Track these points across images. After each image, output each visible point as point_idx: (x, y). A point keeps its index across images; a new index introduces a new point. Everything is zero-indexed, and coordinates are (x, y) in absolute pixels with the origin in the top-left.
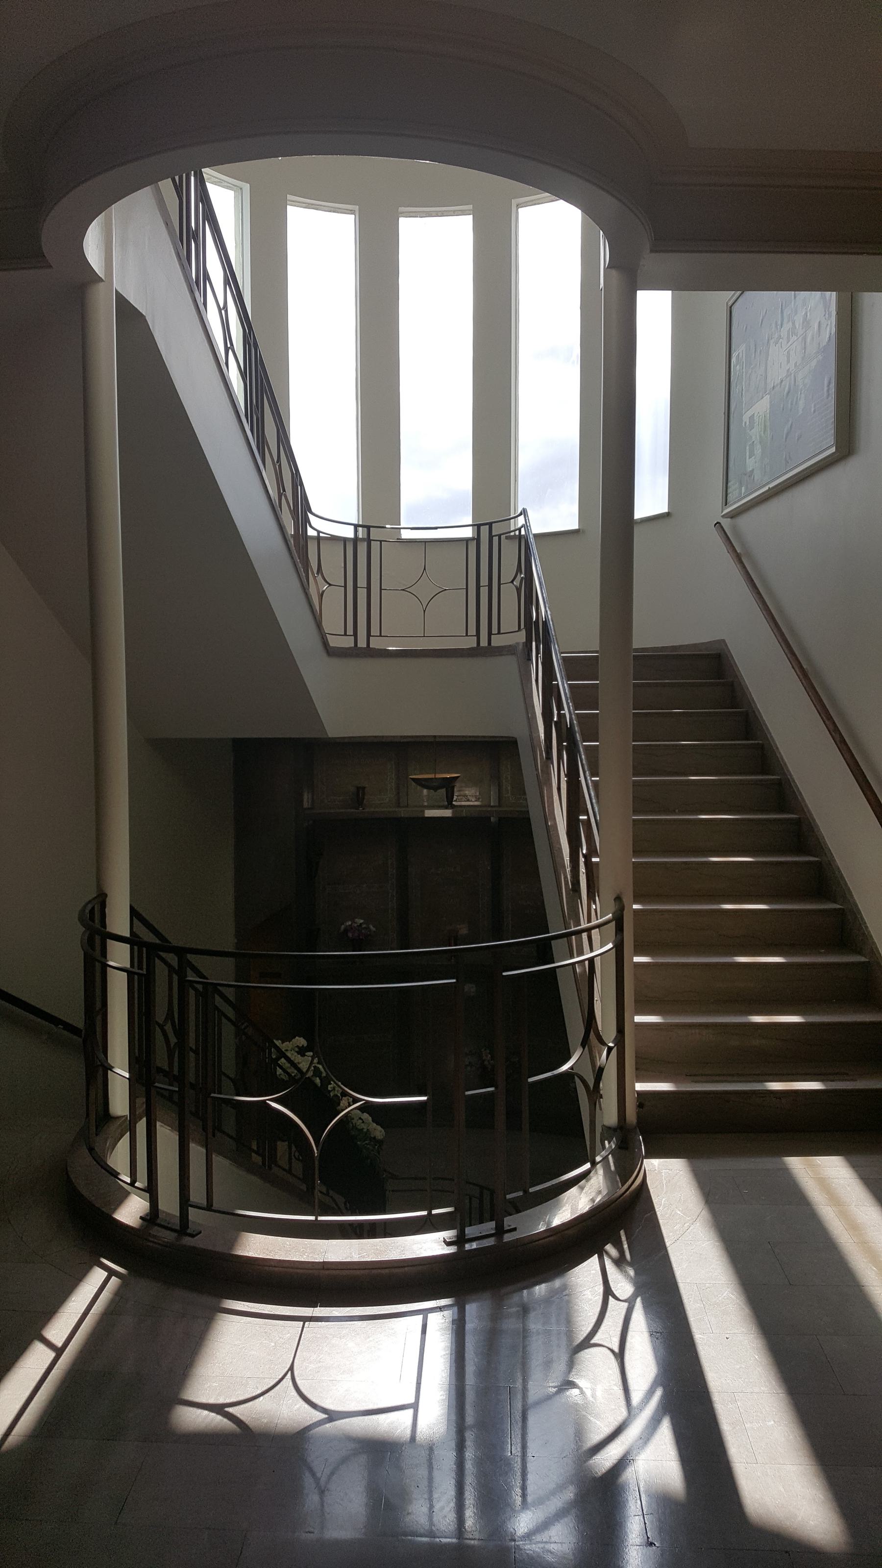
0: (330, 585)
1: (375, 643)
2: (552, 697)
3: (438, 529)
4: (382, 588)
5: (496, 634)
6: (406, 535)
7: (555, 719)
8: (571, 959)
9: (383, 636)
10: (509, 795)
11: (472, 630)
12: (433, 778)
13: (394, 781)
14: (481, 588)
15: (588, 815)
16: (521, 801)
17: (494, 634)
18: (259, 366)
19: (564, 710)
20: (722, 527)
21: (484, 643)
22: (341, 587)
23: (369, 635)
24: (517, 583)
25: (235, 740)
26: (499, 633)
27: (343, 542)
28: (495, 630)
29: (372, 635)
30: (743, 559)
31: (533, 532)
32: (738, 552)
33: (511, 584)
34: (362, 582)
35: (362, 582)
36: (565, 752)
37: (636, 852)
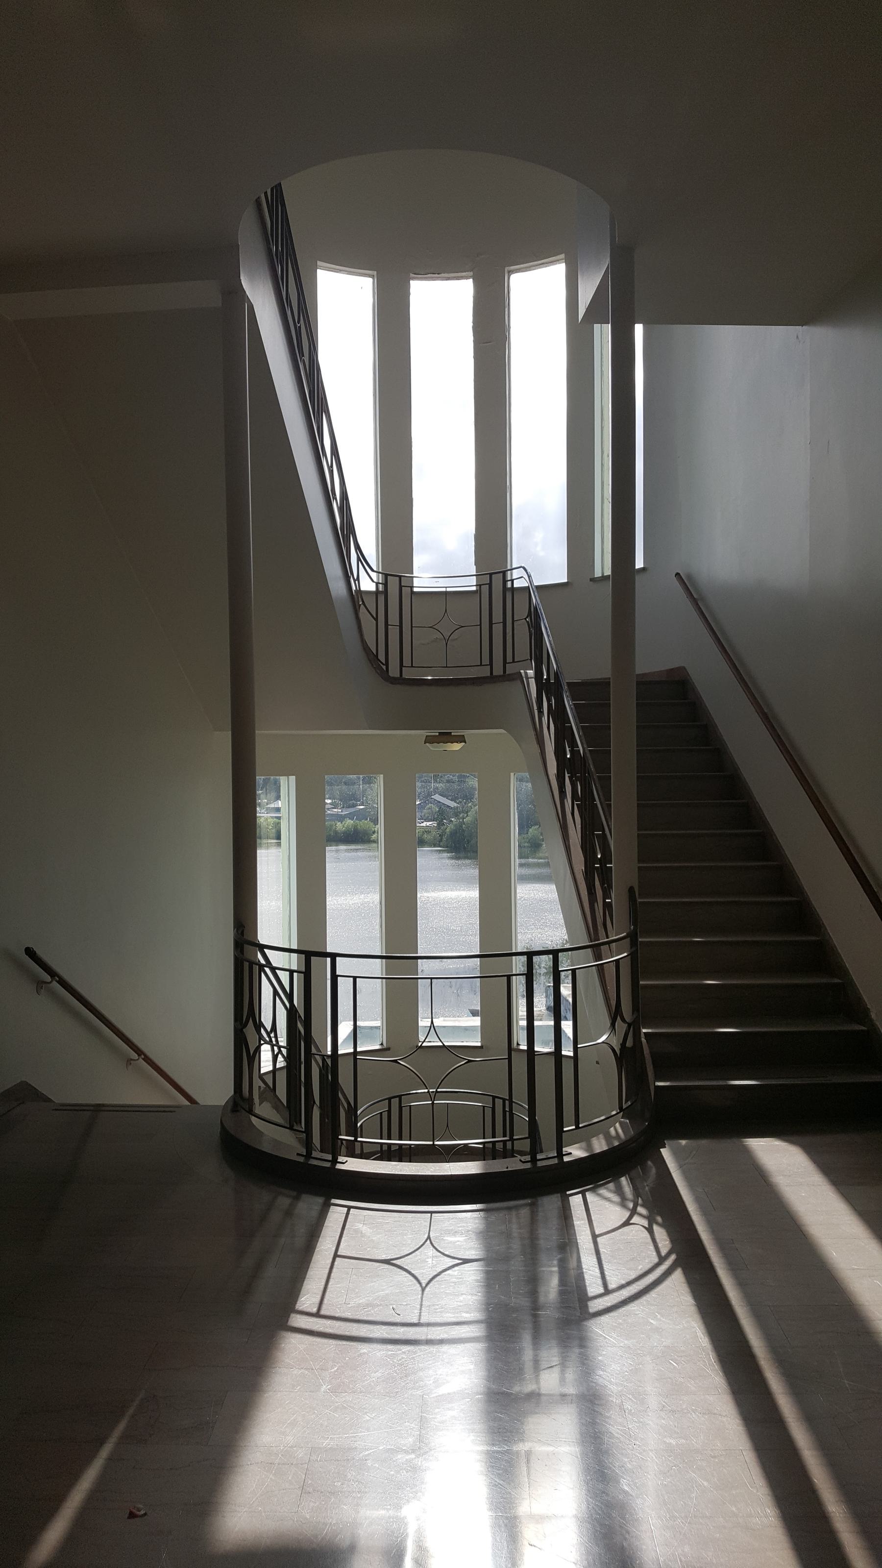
1: (408, 674)
2: (542, 665)
5: (511, 663)
7: (545, 677)
8: (612, 958)
14: (493, 625)
15: (603, 831)
17: (508, 663)
19: (595, 801)
20: (681, 577)
21: (498, 671)
26: (514, 662)
27: (375, 595)
28: (509, 659)
29: (404, 665)
30: (699, 602)
31: (535, 585)
32: (695, 597)
36: (553, 698)
37: (639, 861)
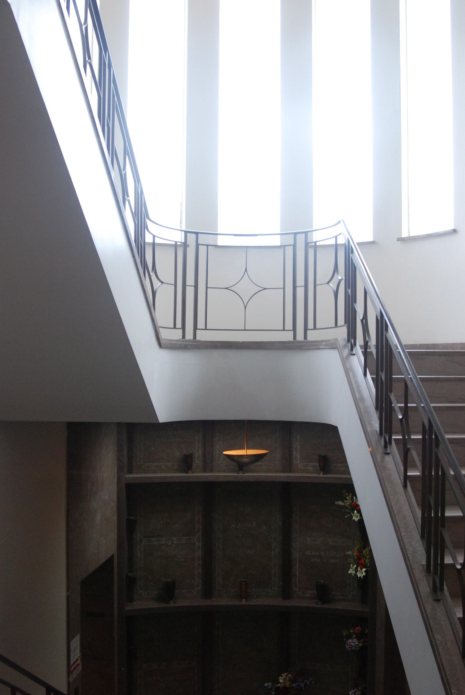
0: (162, 283)
3: (258, 236)
4: (208, 286)
6: (222, 241)
9: (209, 330)
10: (298, 462)
11: (289, 326)
12: (245, 455)
13: (201, 450)
16: (309, 468)
18: (112, 84)
22: (188, 285)
23: (195, 328)
24: (333, 285)
25: (70, 425)
26: (315, 328)
28: (310, 325)
33: (327, 285)
34: (190, 280)
35: (190, 280)
